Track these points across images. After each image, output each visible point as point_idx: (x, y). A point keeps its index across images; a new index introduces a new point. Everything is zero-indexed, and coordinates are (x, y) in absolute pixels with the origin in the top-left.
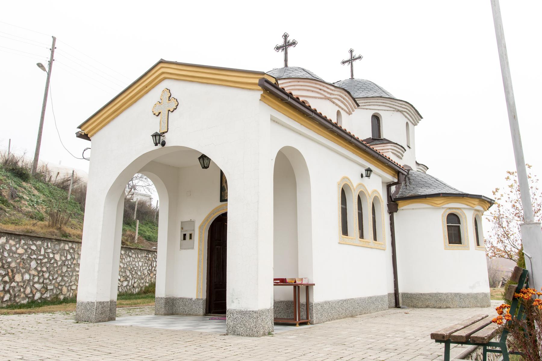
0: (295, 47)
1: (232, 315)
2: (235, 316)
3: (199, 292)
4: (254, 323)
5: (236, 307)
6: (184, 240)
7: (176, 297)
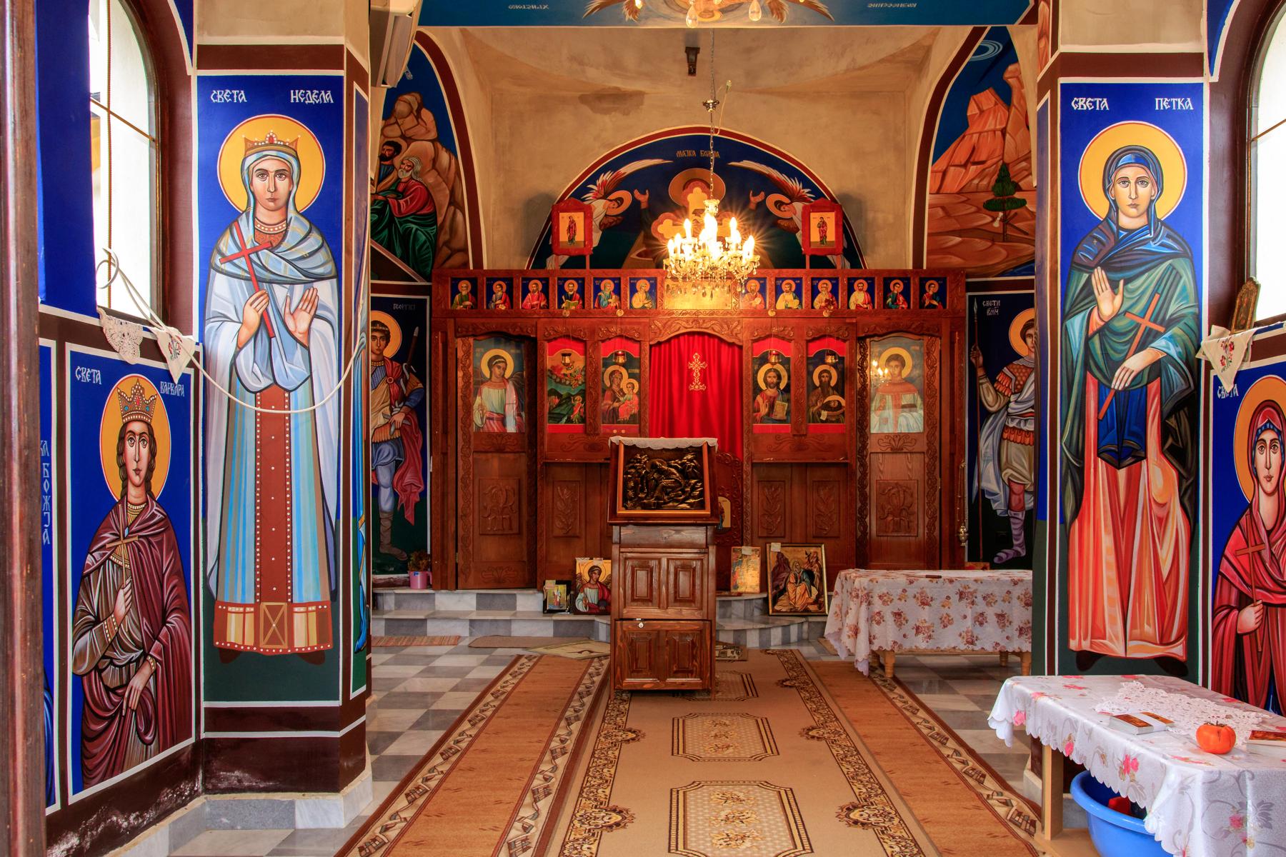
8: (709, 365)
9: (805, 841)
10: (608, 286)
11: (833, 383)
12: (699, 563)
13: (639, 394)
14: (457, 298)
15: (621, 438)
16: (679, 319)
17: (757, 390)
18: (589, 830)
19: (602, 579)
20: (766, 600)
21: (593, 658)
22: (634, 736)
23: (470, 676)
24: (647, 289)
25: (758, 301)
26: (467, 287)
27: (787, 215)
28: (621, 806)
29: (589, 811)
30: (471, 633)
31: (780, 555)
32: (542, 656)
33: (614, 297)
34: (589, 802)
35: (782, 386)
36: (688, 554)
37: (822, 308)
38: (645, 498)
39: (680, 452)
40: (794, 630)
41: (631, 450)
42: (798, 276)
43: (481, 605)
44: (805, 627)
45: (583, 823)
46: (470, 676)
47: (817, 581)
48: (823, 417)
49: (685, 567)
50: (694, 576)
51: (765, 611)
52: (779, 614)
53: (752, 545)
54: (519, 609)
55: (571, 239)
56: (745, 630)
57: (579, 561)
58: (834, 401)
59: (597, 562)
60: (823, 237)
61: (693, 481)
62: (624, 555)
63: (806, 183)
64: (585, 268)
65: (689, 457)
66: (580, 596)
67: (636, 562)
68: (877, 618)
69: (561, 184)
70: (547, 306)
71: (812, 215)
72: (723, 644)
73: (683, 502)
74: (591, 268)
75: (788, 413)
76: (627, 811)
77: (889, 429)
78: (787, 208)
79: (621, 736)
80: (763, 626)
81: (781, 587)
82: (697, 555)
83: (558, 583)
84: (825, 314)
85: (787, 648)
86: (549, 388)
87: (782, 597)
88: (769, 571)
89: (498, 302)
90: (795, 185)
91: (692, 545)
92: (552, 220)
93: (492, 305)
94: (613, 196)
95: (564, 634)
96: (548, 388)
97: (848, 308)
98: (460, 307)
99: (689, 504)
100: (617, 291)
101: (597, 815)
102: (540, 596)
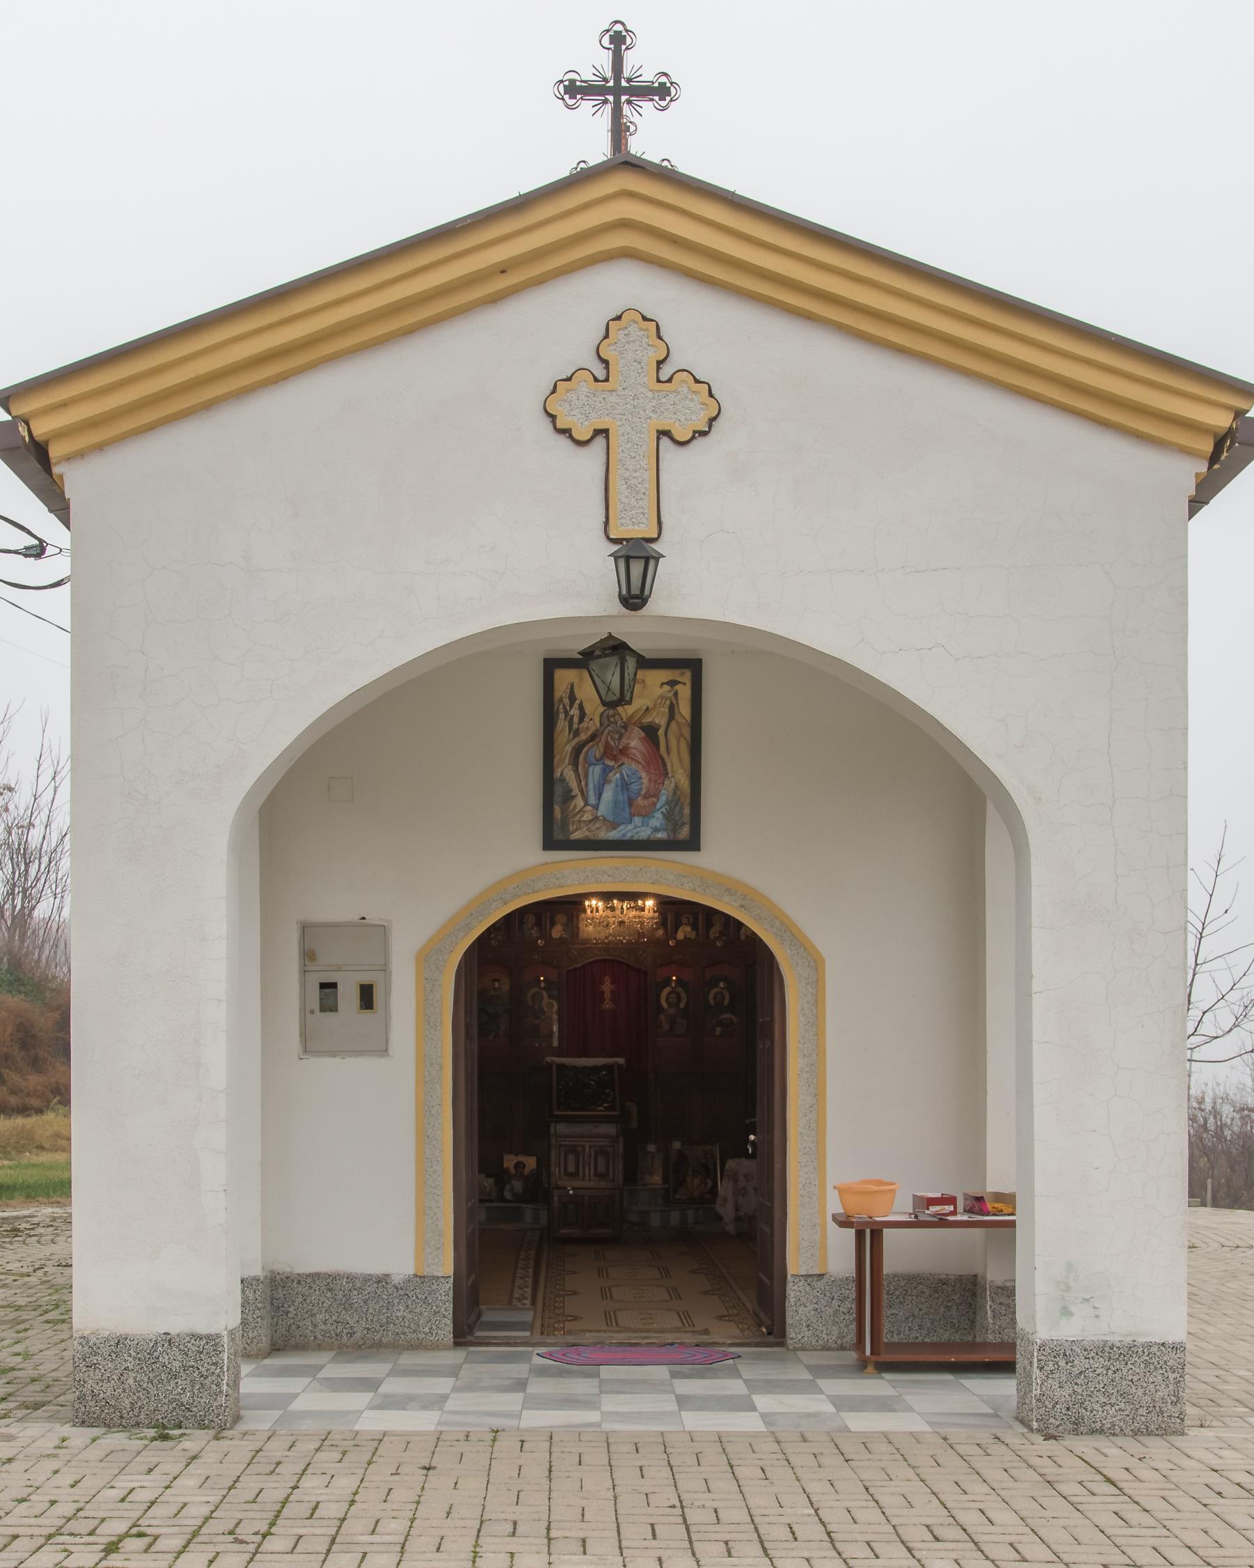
0: (664, 109)
1: (1062, 1363)
2: (1080, 1363)
3: (428, 1250)
4: (1167, 1386)
5: (1083, 1331)
6: (323, 1009)
7: (288, 1270)
11: (726, 1002)
15: (554, 1059)
19: (527, 1171)
33: (535, 928)
35: (682, 1005)
37: (716, 939)
39: (596, 1069)
40: (690, 1213)
41: (561, 1067)
57: (506, 1157)
59: (521, 1158)
61: (607, 1091)
65: (604, 1073)
66: (508, 1187)
91: (606, 1136)
97: (739, 938)
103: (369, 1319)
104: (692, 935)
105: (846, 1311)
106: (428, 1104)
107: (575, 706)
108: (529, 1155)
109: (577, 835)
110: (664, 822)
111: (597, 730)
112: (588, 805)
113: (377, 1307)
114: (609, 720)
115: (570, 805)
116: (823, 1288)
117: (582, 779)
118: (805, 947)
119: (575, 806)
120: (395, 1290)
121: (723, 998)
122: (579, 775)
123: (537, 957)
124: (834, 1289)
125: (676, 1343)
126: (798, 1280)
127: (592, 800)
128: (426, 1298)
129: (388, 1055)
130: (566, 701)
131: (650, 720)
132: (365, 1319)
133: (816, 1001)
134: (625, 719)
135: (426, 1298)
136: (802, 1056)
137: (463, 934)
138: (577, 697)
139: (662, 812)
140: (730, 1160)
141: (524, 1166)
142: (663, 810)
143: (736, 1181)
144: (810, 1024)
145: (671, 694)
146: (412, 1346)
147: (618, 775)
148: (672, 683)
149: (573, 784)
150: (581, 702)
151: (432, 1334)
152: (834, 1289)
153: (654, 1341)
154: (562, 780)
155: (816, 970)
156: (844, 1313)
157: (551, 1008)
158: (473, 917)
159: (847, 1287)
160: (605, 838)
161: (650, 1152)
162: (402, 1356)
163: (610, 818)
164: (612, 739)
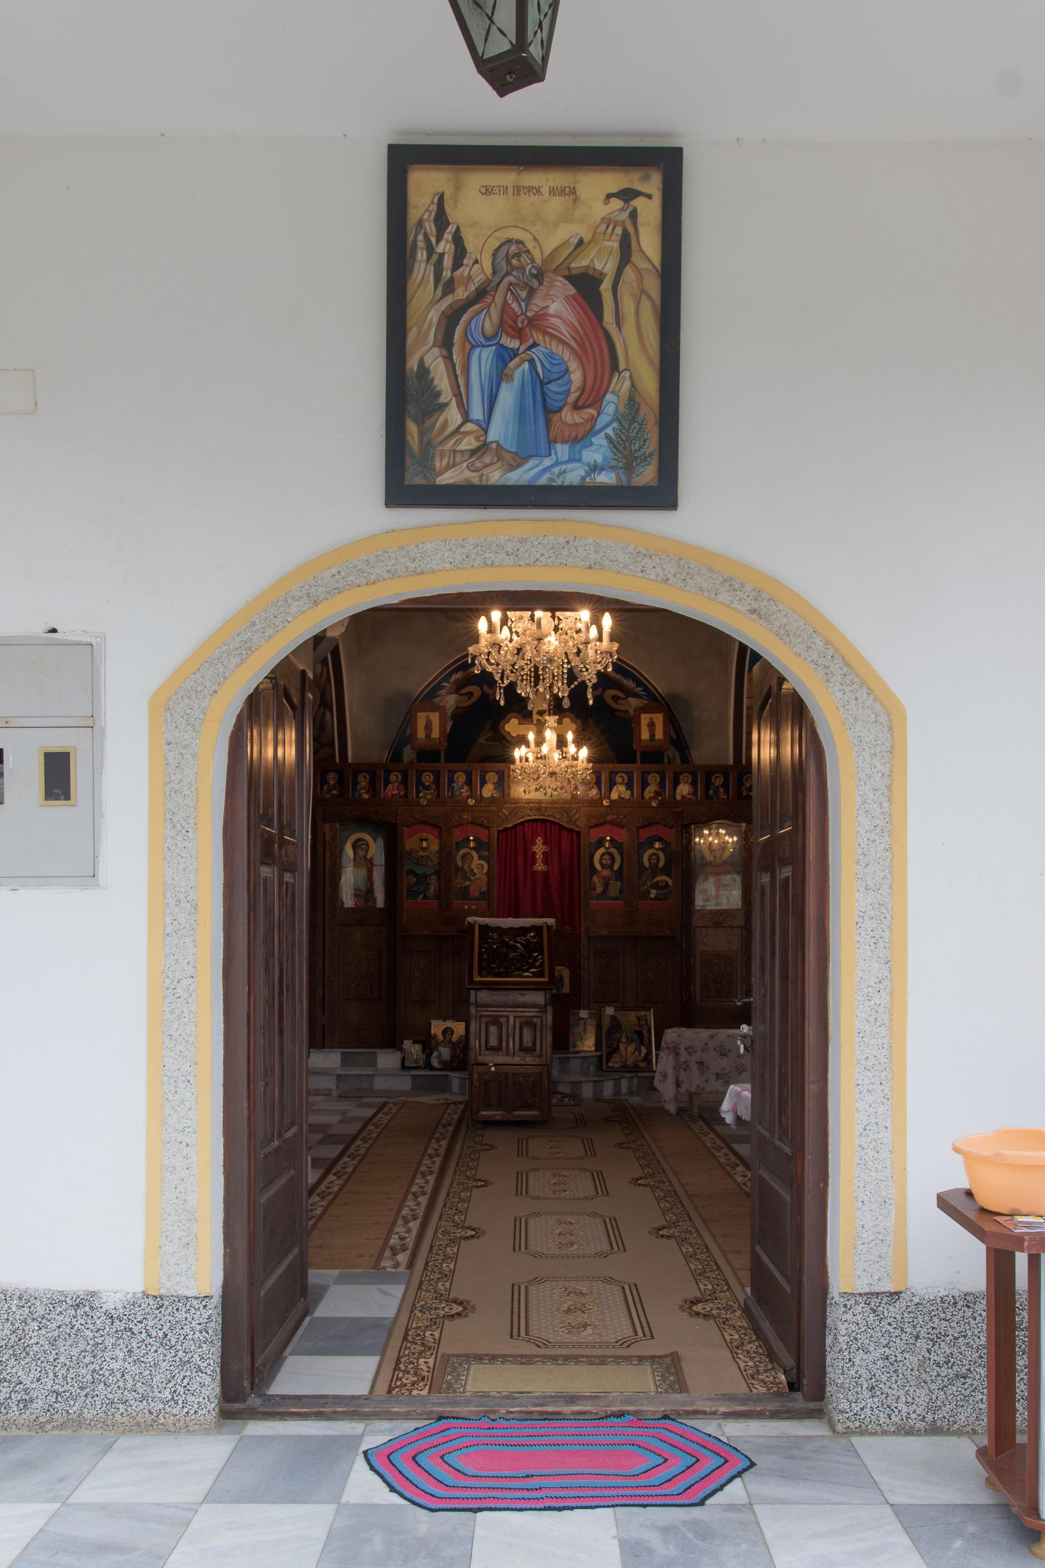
8: (551, 849)
9: (646, 1329)
10: (461, 778)
11: (661, 864)
12: (539, 1020)
13: (488, 874)
14: (325, 787)
15: (476, 919)
16: (523, 807)
17: (593, 870)
18: (431, 1319)
19: (454, 1039)
20: (600, 1057)
21: (449, 1104)
22: (461, 1309)
23: (348, 1115)
24: (496, 781)
25: (594, 792)
26: (334, 778)
27: (623, 708)
28: (462, 1297)
29: (430, 1301)
30: (338, 1087)
31: (613, 1019)
32: (405, 1102)
34: (428, 1294)
35: (616, 867)
36: (530, 1013)
37: (651, 799)
38: (496, 968)
39: (523, 931)
40: (624, 1083)
41: (485, 929)
42: (630, 770)
43: (345, 1061)
44: (635, 1081)
45: (424, 1313)
46: (348, 1115)
47: (646, 1040)
48: (652, 896)
49: (528, 1023)
50: (535, 1030)
51: (599, 1068)
52: (612, 1070)
53: (589, 1009)
54: (379, 1065)
55: (428, 736)
56: (580, 1082)
57: (434, 1023)
58: (662, 881)
59: (449, 1024)
60: (652, 735)
61: (535, 954)
62: (480, 1013)
63: (639, 683)
64: (439, 761)
65: (532, 934)
66: (435, 1054)
67: (489, 1019)
68: (684, 1066)
69: (418, 685)
70: (406, 796)
71: (643, 716)
72: (562, 1093)
73: (527, 971)
74: (446, 761)
75: (621, 891)
76: (468, 1302)
77: (711, 906)
78: (622, 702)
79: (460, 1233)
80: (596, 1079)
81: (614, 1046)
82: (537, 1014)
83: (415, 1042)
84: (654, 804)
85: (617, 1098)
86: (407, 868)
87: (615, 1055)
88: (604, 1032)
89: (362, 791)
90: (630, 684)
92: (410, 720)
93: (357, 794)
94: (464, 691)
95: (421, 1086)
96: (406, 868)
98: (328, 796)
99: (531, 973)
100: (469, 782)
101: (438, 1306)
102: (398, 1055)
103: (60, 1374)
104: (627, 795)
105: (941, 1359)
106: (170, 974)
107: (446, 236)
108: (458, 1021)
109: (447, 478)
110: (609, 454)
111: (488, 282)
112: (471, 421)
113: (75, 1352)
114: (508, 262)
115: (435, 422)
116: (899, 1317)
117: (458, 372)
118: (869, 688)
119: (446, 423)
120: (108, 1322)
121: (658, 859)
122: (454, 365)
123: (466, 817)
124: (920, 1318)
125: (628, 1413)
126: (852, 1302)
127: (477, 412)
128: (166, 1335)
129: (97, 885)
130: (430, 227)
131: (585, 263)
132: (51, 1375)
133: (889, 788)
134: (538, 261)
135: (166, 1335)
136: (862, 889)
137: (237, 660)
138: (451, 221)
139: (607, 436)
140: (670, 1031)
141: (453, 1032)
142: (609, 431)
143: (677, 1054)
144: (879, 829)
145: (625, 216)
146: (138, 1425)
147: (526, 365)
148: (627, 195)
149: (441, 381)
150: (458, 229)
151: (177, 1403)
152: (920, 1318)
153: (588, 1408)
154: (423, 371)
155: (890, 729)
156: (938, 1365)
157: (478, 866)
158: (256, 628)
159: (942, 1315)
160: (500, 483)
161: (583, 1018)
162: (108, 1460)
163: (510, 445)
164: (516, 298)
